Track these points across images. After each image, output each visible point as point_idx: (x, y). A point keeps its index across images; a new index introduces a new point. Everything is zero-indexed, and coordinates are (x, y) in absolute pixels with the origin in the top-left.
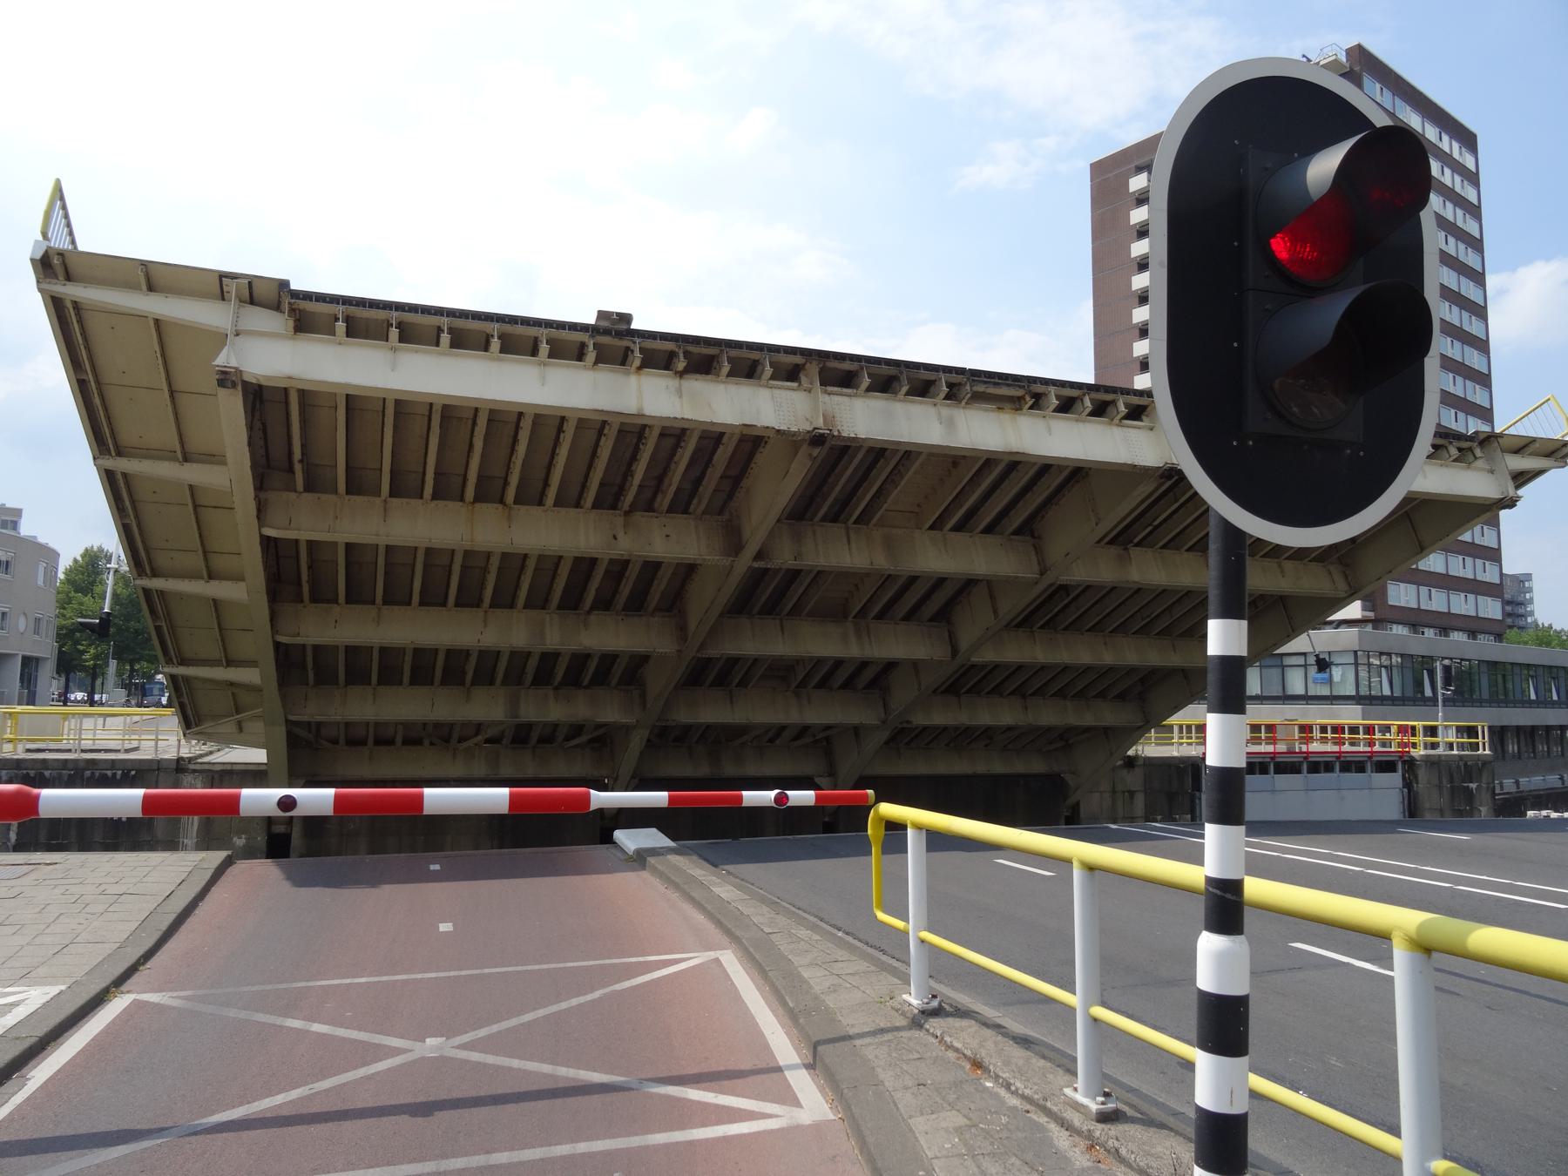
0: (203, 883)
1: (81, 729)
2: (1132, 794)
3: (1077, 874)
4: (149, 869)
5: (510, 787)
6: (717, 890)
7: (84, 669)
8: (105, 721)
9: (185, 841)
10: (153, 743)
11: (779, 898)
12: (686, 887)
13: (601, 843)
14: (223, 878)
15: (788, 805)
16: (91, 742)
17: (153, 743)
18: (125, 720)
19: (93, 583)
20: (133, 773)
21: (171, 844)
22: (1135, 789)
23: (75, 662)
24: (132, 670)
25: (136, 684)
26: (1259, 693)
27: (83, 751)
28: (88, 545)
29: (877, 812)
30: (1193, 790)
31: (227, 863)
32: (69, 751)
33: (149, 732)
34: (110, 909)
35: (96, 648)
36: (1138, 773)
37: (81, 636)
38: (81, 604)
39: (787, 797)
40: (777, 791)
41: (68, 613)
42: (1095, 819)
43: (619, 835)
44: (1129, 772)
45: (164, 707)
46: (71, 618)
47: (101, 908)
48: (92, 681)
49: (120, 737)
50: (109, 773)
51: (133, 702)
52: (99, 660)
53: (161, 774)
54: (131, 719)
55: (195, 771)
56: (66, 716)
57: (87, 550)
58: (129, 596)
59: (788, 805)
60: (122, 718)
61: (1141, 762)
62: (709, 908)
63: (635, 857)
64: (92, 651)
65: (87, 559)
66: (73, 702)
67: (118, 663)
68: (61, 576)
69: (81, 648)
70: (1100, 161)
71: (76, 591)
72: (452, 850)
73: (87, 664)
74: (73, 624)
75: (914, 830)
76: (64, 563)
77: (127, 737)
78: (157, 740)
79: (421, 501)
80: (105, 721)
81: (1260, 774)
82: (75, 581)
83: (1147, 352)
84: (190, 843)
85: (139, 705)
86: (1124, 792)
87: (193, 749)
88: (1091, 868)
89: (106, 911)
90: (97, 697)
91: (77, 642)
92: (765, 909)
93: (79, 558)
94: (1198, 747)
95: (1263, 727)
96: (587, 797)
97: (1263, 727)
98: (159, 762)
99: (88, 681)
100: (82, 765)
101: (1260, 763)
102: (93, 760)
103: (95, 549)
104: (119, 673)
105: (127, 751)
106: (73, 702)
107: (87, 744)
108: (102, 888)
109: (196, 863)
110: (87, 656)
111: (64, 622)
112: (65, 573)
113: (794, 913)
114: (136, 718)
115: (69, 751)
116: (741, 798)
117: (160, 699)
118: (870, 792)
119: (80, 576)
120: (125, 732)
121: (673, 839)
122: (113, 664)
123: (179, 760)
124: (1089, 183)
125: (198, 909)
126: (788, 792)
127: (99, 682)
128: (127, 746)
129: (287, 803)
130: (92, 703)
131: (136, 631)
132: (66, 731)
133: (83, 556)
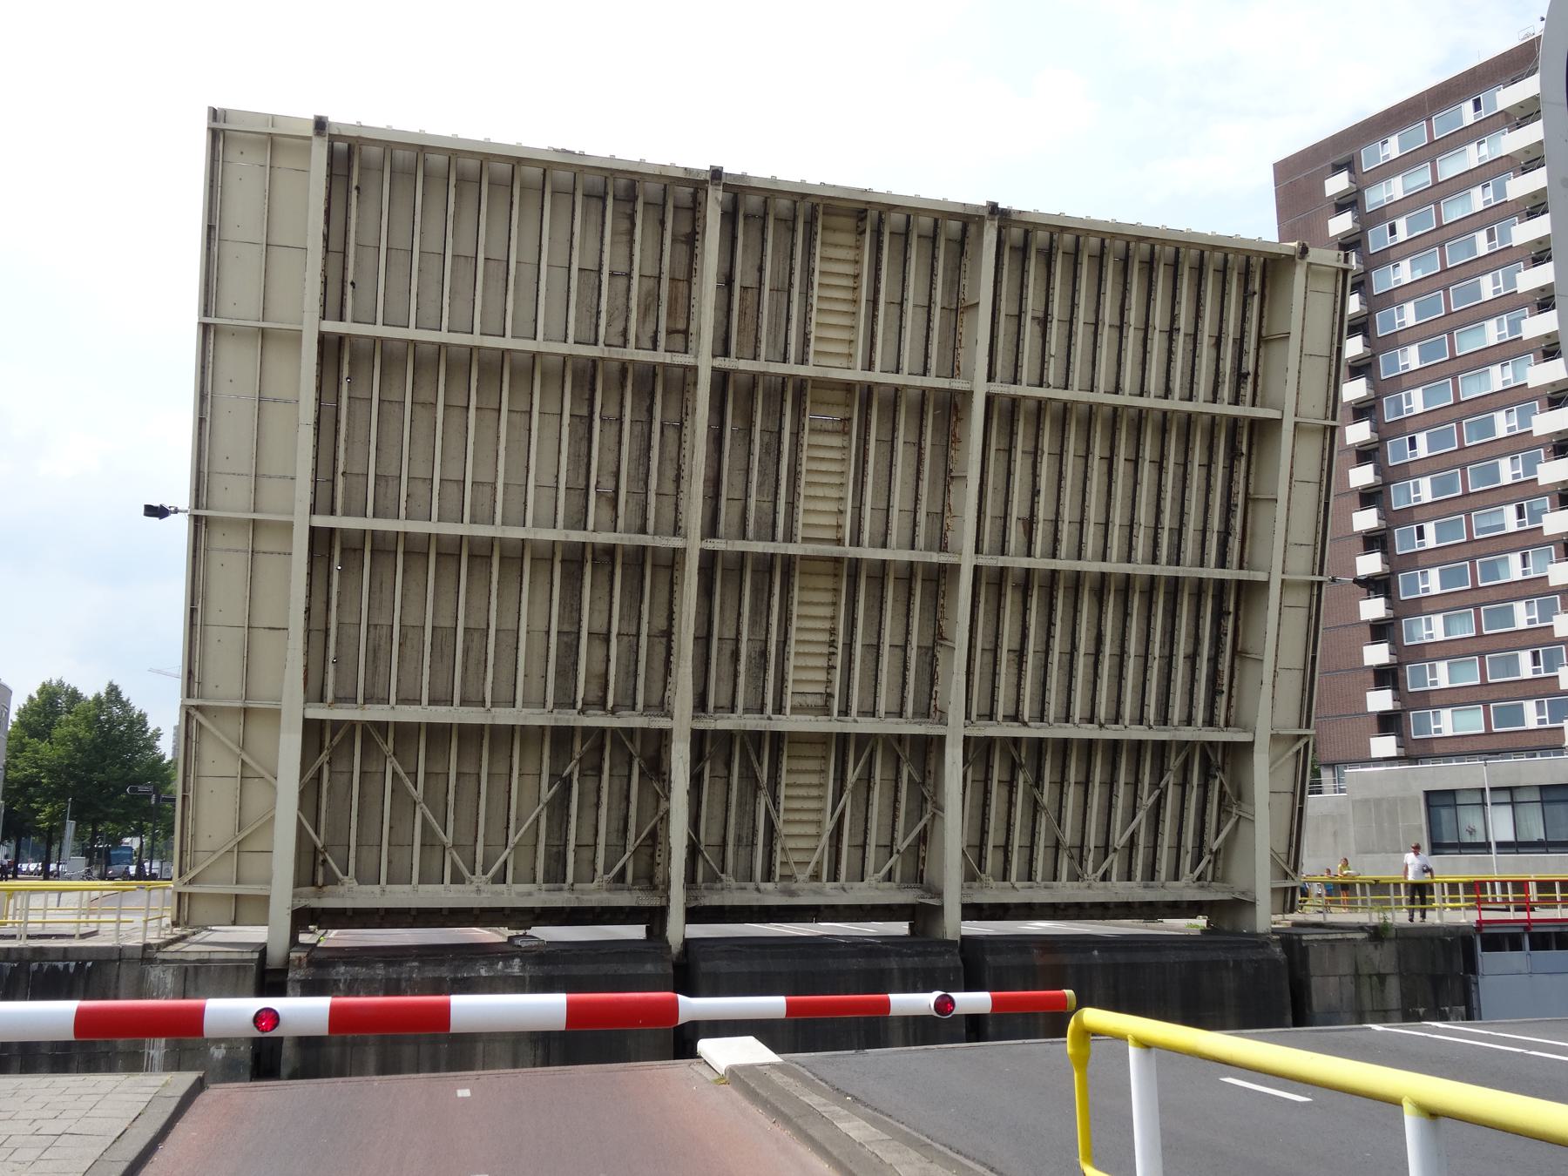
0: (166, 1117)
1: (28, 909)
2: (1382, 978)
3: (1411, 1123)
4: (95, 1098)
5: (567, 992)
6: (843, 1126)
7: (39, 832)
8: (59, 897)
9: (152, 1052)
10: (113, 926)
11: (928, 1137)
12: (800, 1122)
13: (676, 1058)
14: (192, 1110)
15: (954, 1013)
16: (40, 925)
17: (113, 926)
18: (82, 895)
19: (50, 726)
20: (89, 964)
21: (135, 1063)
22: (1387, 972)
23: (27, 824)
24: (95, 833)
25: (99, 850)
26: (1543, 837)
27: (29, 937)
28: (46, 680)
29: (1079, 1022)
30: (1466, 972)
31: (198, 1087)
32: (13, 937)
33: (110, 911)
34: (46, 1155)
35: (53, 806)
36: (1389, 949)
37: (35, 792)
38: (36, 752)
39: (952, 1001)
40: (938, 994)
41: (20, 763)
42: (1331, 1018)
43: (705, 1046)
44: (1376, 947)
45: (132, 878)
46: (24, 769)
47: (31, 1154)
48: (46, 850)
49: (74, 918)
50: (60, 965)
51: (95, 873)
52: (55, 821)
53: (123, 966)
54: (90, 895)
55: (164, 961)
56: (12, 893)
57: (44, 685)
58: (93, 740)
59: (954, 1013)
60: (78, 893)
61: (1392, 934)
62: (835, 1153)
63: (727, 1077)
64: (47, 810)
65: (44, 696)
66: (24, 873)
67: (77, 825)
68: (13, 717)
69: (35, 806)
70: (1286, 160)
71: (31, 737)
72: (483, 1069)
73: (42, 825)
74: (26, 776)
75: (1139, 1049)
76: (18, 702)
77: (83, 918)
78: (119, 922)
79: (493, 527)
80: (59, 897)
81: (1558, 949)
82: (30, 724)
83: (1556, 328)
84: (157, 1054)
85: (103, 877)
86: (1370, 976)
87: (162, 932)
88: (1432, 1115)
89: (39, 1159)
90: (53, 867)
91: (31, 799)
92: (914, 1155)
93: (35, 696)
94: (1468, 913)
95: (1557, 884)
96: (674, 1005)
97: (1557, 884)
98: (121, 950)
99: (43, 848)
100: (28, 955)
101: (1556, 933)
102: (41, 948)
103: (54, 683)
104: (78, 836)
105: (83, 936)
106: (24, 873)
107: (35, 929)
108: (36, 1125)
109: (157, 1089)
110: (41, 816)
111: (16, 775)
112: (19, 715)
113: (954, 1160)
114: (95, 894)
115: (13, 937)
116: (887, 1003)
117: (128, 868)
118: (1069, 993)
119: (36, 718)
120: (81, 912)
121: (776, 1049)
122: (71, 826)
123: (146, 947)
124: (1274, 188)
125: (157, 1153)
126: (955, 995)
127: (55, 848)
128: (84, 930)
129: (267, 1018)
130: (46, 874)
131: (100, 784)
132: (11, 912)
133: (40, 693)
